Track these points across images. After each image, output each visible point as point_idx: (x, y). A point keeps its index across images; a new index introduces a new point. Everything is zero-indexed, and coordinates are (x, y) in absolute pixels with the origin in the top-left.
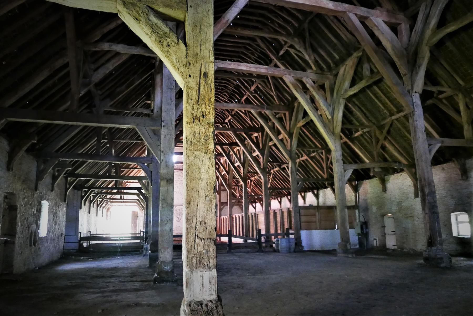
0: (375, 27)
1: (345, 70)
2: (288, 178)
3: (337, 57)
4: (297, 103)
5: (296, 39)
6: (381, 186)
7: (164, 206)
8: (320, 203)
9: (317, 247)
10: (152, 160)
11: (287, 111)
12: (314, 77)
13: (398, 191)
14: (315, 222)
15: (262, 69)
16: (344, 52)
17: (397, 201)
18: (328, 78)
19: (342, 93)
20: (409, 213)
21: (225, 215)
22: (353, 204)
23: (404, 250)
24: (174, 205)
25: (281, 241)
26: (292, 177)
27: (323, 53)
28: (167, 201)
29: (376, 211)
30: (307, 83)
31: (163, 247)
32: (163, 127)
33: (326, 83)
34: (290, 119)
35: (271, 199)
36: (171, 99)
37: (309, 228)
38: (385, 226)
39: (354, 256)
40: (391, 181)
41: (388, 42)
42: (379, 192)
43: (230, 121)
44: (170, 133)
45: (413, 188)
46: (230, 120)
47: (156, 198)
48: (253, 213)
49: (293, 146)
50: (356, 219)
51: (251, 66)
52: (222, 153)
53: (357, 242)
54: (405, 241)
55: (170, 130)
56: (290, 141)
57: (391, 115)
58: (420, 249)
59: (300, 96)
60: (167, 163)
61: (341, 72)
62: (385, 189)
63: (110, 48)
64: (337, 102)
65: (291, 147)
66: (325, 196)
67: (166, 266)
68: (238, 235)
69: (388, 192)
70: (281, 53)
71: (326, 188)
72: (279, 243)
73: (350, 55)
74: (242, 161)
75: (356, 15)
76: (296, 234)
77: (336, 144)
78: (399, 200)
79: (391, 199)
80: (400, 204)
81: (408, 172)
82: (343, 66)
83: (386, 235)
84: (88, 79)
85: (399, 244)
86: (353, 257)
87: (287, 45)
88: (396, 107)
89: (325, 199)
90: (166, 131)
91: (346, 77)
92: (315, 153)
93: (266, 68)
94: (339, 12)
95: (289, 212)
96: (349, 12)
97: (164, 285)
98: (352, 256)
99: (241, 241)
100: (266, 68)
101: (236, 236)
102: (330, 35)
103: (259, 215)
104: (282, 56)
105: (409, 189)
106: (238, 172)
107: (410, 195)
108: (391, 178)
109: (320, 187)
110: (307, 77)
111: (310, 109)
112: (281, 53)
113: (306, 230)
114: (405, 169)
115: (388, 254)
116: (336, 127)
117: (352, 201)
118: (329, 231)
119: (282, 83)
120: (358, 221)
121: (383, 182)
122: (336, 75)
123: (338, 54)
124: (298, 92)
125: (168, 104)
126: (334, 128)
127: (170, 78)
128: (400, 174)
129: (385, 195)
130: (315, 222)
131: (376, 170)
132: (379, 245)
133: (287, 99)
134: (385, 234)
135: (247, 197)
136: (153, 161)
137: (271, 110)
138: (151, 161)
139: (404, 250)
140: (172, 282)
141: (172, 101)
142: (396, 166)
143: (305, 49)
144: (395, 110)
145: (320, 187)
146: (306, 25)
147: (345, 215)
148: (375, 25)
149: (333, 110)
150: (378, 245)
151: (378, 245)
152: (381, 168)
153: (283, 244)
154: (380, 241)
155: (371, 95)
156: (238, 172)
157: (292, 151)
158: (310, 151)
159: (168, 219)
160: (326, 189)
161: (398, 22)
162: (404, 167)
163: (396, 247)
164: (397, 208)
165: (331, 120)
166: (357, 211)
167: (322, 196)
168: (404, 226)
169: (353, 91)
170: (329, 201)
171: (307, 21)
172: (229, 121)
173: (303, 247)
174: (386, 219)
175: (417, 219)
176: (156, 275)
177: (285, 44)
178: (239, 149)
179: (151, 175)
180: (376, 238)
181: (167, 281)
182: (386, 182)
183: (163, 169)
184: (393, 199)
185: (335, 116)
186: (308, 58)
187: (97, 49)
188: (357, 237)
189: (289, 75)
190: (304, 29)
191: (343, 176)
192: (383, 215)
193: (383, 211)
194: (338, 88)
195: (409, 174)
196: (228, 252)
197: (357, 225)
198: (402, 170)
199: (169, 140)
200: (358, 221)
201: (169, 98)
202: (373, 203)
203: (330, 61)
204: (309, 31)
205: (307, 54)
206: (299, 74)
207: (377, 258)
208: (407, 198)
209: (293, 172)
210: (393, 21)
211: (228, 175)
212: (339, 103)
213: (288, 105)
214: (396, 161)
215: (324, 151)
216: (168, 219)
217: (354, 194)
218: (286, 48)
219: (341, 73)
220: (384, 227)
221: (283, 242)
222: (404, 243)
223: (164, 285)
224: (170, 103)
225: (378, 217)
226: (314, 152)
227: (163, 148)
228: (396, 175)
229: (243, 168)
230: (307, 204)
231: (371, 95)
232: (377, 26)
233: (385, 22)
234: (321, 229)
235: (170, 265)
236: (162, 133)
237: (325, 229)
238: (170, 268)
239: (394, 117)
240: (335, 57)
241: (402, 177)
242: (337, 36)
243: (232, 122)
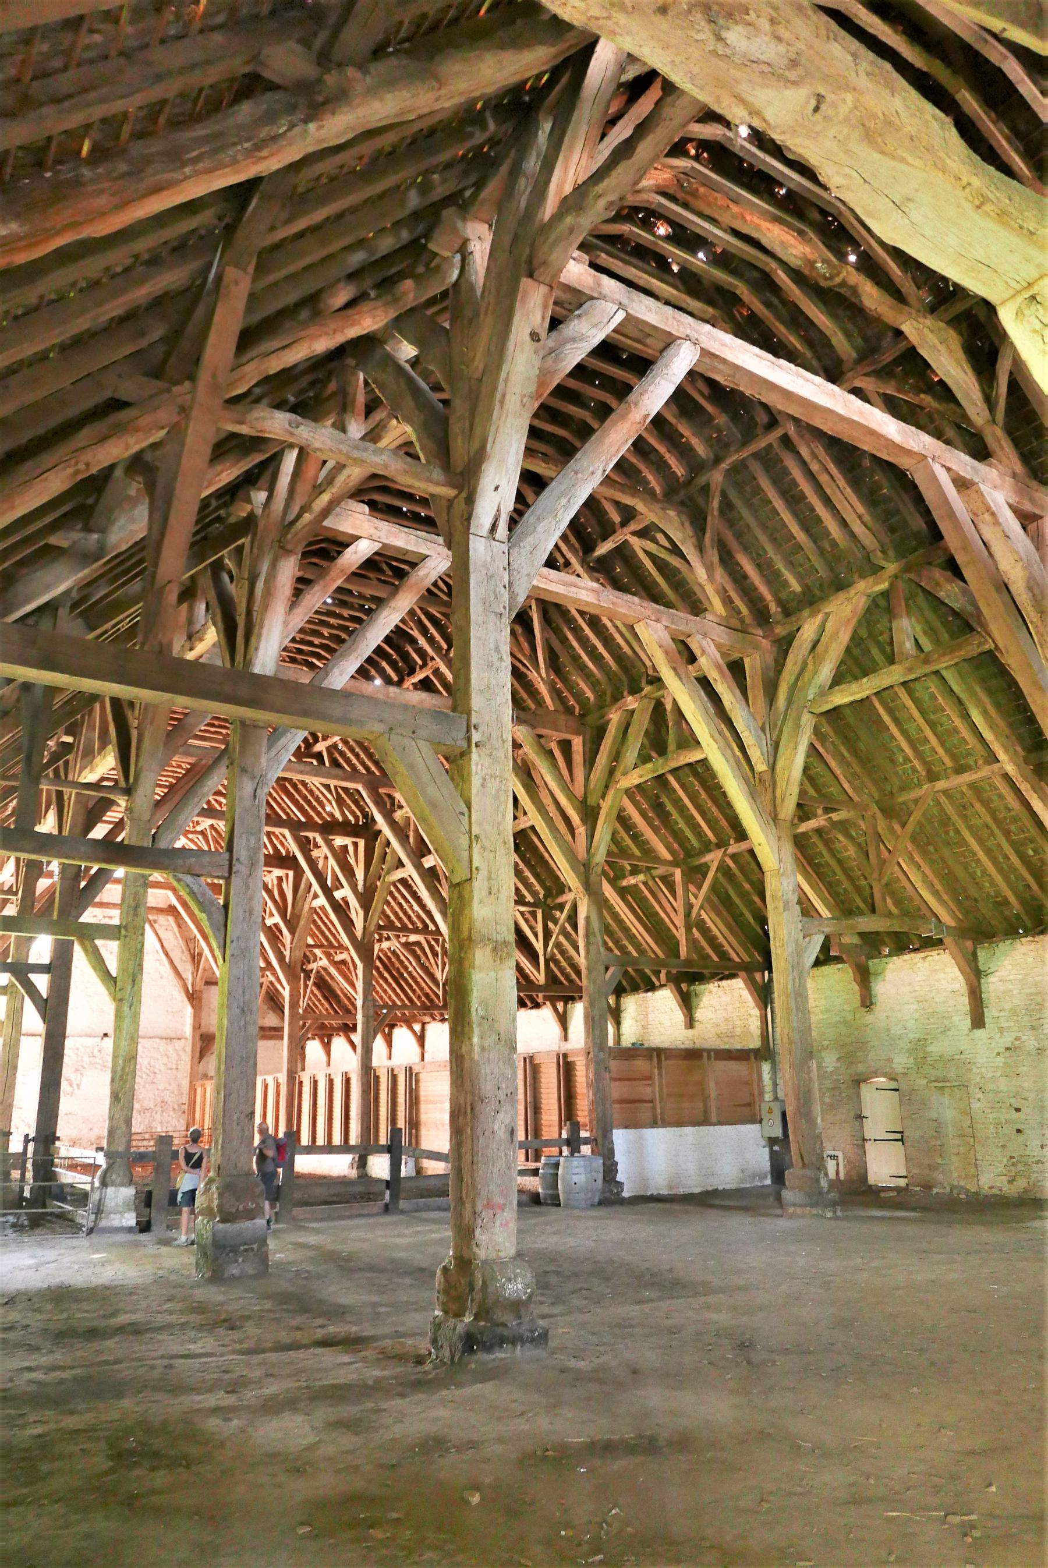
0: (987, 516)
1: (822, 629)
2: (572, 952)
3: (796, 586)
4: (619, 713)
5: (672, 513)
6: (857, 988)
7: (486, 1044)
8: (623, 1038)
9: (659, 1185)
10: (231, 866)
11: (578, 734)
12: (721, 635)
13: (913, 1007)
14: (651, 1101)
15: (583, 592)
16: (823, 572)
17: (911, 1036)
18: (757, 647)
19: (811, 697)
20: (952, 1075)
21: (269, 1073)
22: (756, 1043)
23: (935, 1191)
24: (141, 1033)
25: (565, 1167)
26: (588, 952)
27: (749, 568)
28: (496, 1025)
29: (837, 1068)
30: (704, 652)
31: (489, 1205)
32: (477, 745)
33: (747, 662)
34: (590, 762)
35: (427, 1019)
36: (497, 649)
37: (632, 1124)
38: (864, 1114)
39: (839, 1213)
40: (889, 975)
41: (1019, 565)
42: (847, 1008)
43: (332, 749)
44: (498, 773)
45: (965, 1000)
46: (335, 746)
47: (243, 1011)
48: (399, 1066)
49: (598, 848)
50: (761, 1093)
51: (551, 577)
52: (295, 857)
53: (766, 1166)
54: (939, 1161)
55: (496, 761)
56: (584, 833)
57: (932, 777)
58: (991, 1188)
59: (685, 690)
60: (493, 882)
61: (808, 631)
62: (867, 1001)
63: (292, 434)
64: (789, 724)
65: (588, 851)
66: (646, 1016)
67: (509, 1280)
68: (337, 1140)
69: (877, 1009)
70: (604, 549)
71: (651, 988)
72: (560, 1172)
73: (840, 585)
74: (360, 887)
75: (949, 469)
76: (600, 1141)
77: (782, 854)
78: (917, 1036)
79: (888, 1030)
80: (919, 1048)
81: (955, 950)
82: (813, 615)
83: (868, 1145)
84: (96, 536)
85: (915, 1171)
86: (836, 1218)
87: (633, 526)
88: (953, 756)
89: (644, 1027)
90: (487, 761)
91: (826, 651)
92: (641, 877)
93: (593, 591)
94: (908, 452)
95: (566, 1067)
96: (933, 458)
97: (503, 1355)
98: (835, 1212)
99: (340, 1165)
100: (593, 591)
101: (312, 1149)
102: (786, 516)
103: (421, 1076)
104: (601, 560)
105: (952, 1003)
106: (348, 924)
107: (956, 1019)
108: (890, 966)
109: (628, 988)
110: (705, 635)
111: (712, 736)
112: (604, 549)
113: (626, 1127)
114: (948, 941)
115: (884, 1204)
116: (783, 800)
117: (747, 1032)
118: (688, 1130)
119: (575, 644)
120: (768, 1097)
121: (864, 977)
122: (784, 645)
123: (799, 577)
124: (680, 679)
125: (490, 665)
126: (778, 801)
127: (492, 576)
128: (923, 955)
129: (869, 1018)
130: (651, 1101)
131: (846, 940)
132: (847, 1174)
133: (579, 696)
134: (864, 1140)
135: (371, 1013)
136: (234, 869)
137: (534, 727)
138: (226, 868)
139: (935, 1191)
140: (532, 1340)
141: (501, 659)
142: (928, 931)
143: (700, 548)
144: (949, 763)
145: (628, 988)
146: (717, 477)
147: (810, 1080)
148: (988, 509)
149: (776, 746)
150: (842, 1176)
151: (842, 1176)
152: (861, 935)
153: (576, 1179)
154: (849, 1161)
155: (881, 711)
156: (348, 924)
157: (593, 864)
158: (622, 869)
159: (501, 1095)
160: (650, 994)
161: (1037, 512)
162: (948, 935)
163: (902, 1183)
164: (912, 1060)
165: (767, 777)
166: (766, 1067)
167: (633, 1014)
168: (935, 1116)
169: (852, 694)
170: (663, 1031)
171: (724, 466)
172: (328, 749)
173: (620, 1184)
174: (867, 1092)
175: (980, 1095)
176: (468, 1319)
177: (624, 524)
178: (346, 846)
179: (222, 920)
180: (833, 1153)
181: (514, 1340)
182: (872, 978)
183: (481, 902)
184: (896, 1030)
185: (780, 765)
186: (705, 577)
187: (244, 430)
188: (767, 1150)
189: (658, 621)
190: (706, 489)
191: (799, 953)
192: (858, 1081)
193: (861, 1068)
194: (792, 681)
195: (960, 957)
196: (387, 1209)
197: (770, 1111)
198: (732, 976)
199: (497, 797)
200: (768, 1097)
201: (492, 646)
202: (826, 1043)
203: (768, 597)
204: (724, 494)
205: (704, 565)
206: (683, 620)
207: (904, 1219)
208: (946, 1030)
209: (594, 934)
210: (1027, 507)
211: (292, 932)
212: (797, 725)
213: (582, 716)
214: (927, 914)
215: (678, 874)
216: (501, 1095)
217: (756, 1012)
218: (623, 535)
219: (805, 636)
220: (860, 1117)
221: (576, 1171)
222: (933, 1167)
223: (503, 1355)
224: (497, 663)
225: (843, 1086)
226: (635, 871)
227: (480, 824)
228: (907, 957)
229: (361, 913)
230: (627, 1040)
231: (881, 711)
232: (993, 514)
233: (1010, 506)
234: (665, 1124)
235: (524, 1277)
236: (473, 767)
237: (680, 1124)
238: (528, 1286)
239: (941, 785)
240: (786, 584)
241: (926, 964)
242: (810, 523)
243: (342, 754)
